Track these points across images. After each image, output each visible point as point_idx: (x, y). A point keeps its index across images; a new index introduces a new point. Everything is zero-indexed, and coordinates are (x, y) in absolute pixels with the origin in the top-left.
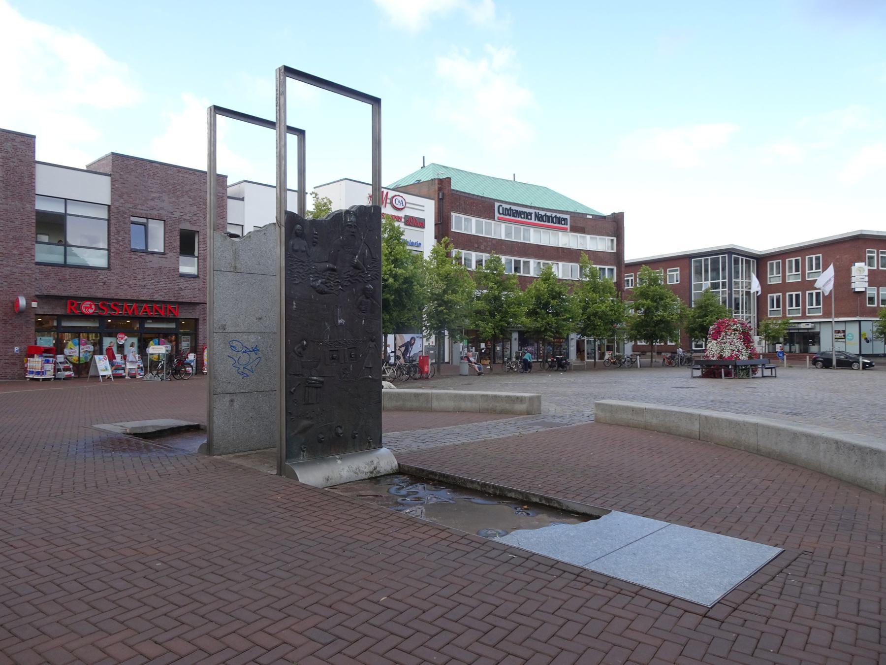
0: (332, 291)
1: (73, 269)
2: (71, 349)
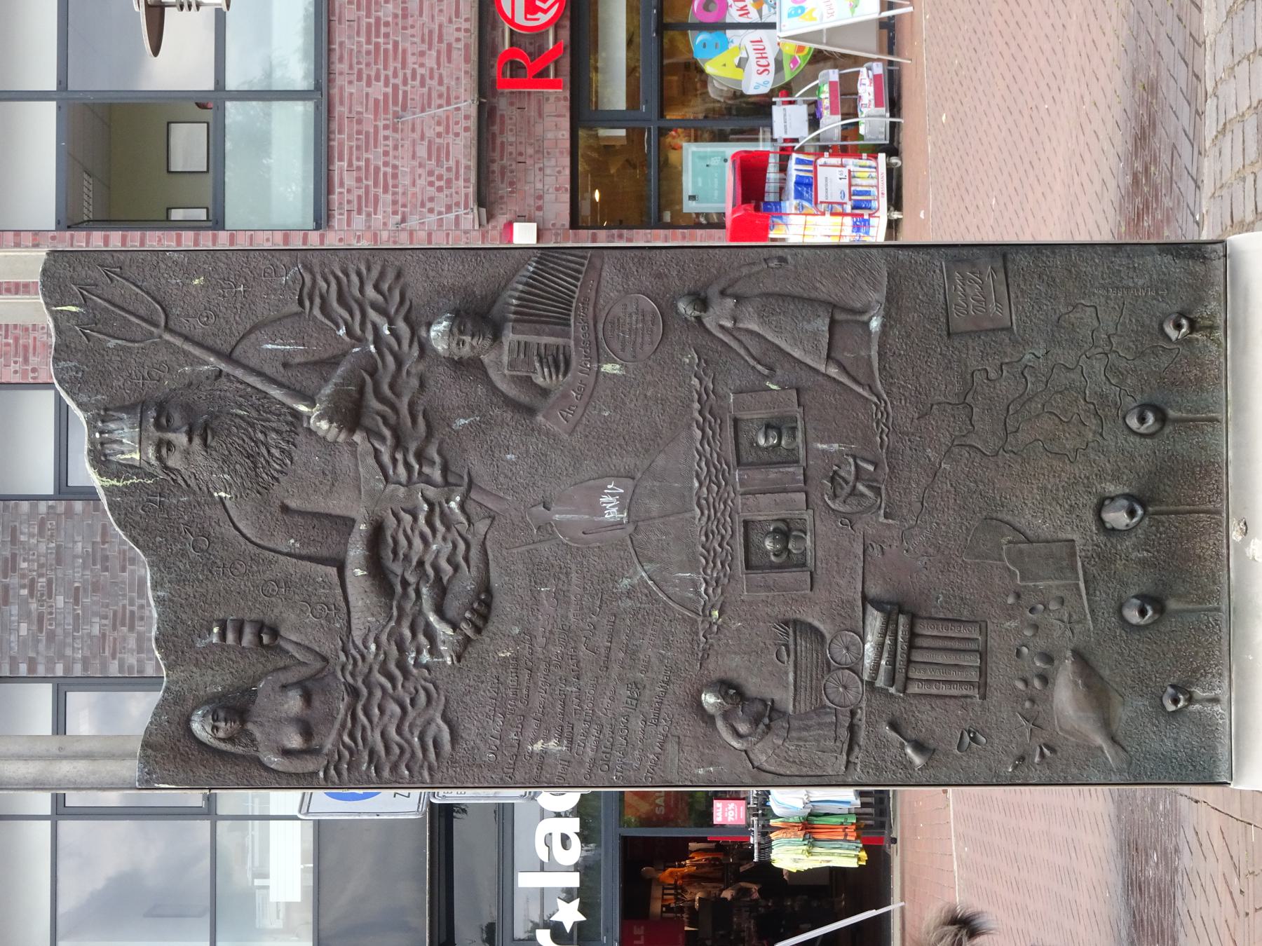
0: (474, 553)
1: (337, 67)
2: (742, 64)
